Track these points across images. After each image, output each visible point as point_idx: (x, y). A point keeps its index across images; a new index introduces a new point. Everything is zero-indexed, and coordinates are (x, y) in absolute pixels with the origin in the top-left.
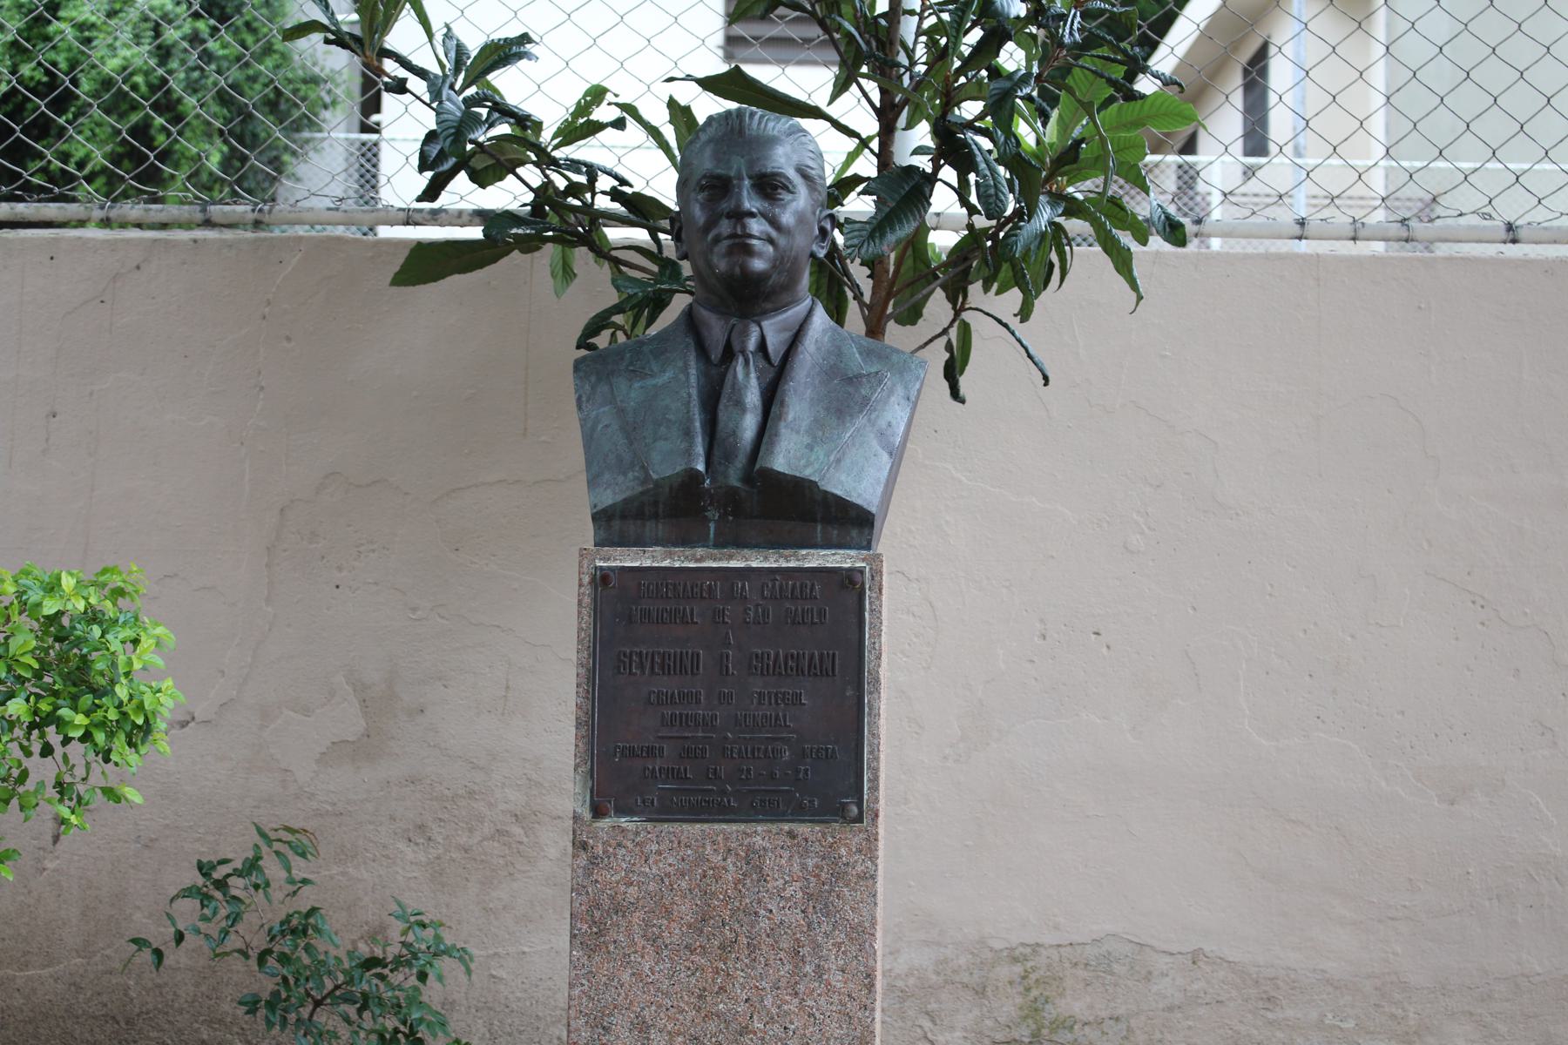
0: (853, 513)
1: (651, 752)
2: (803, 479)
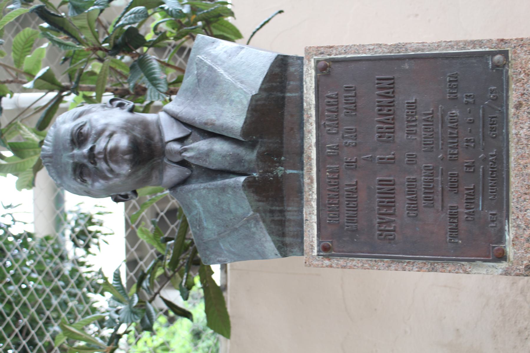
0: (277, 70)
1: (454, 216)
2: (250, 105)
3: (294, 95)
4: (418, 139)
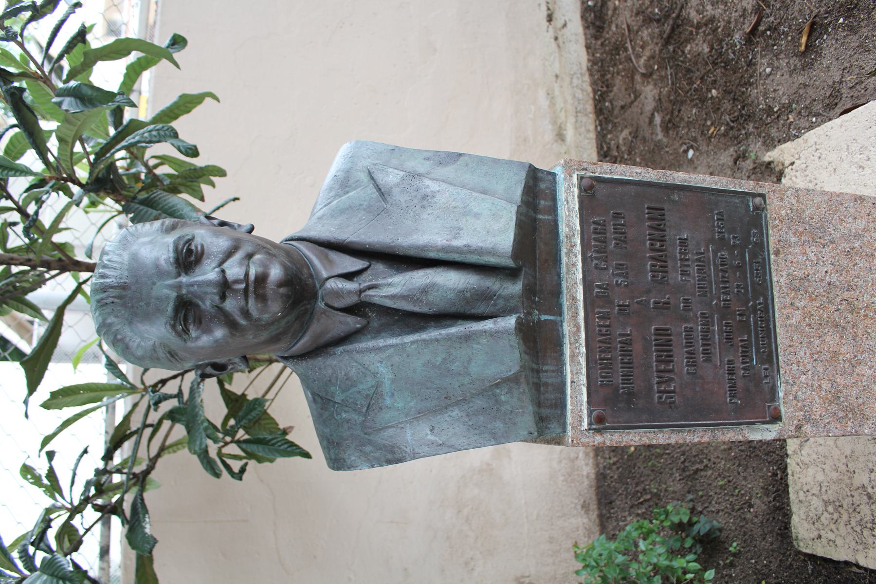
3: (547, 217)
4: (692, 281)
